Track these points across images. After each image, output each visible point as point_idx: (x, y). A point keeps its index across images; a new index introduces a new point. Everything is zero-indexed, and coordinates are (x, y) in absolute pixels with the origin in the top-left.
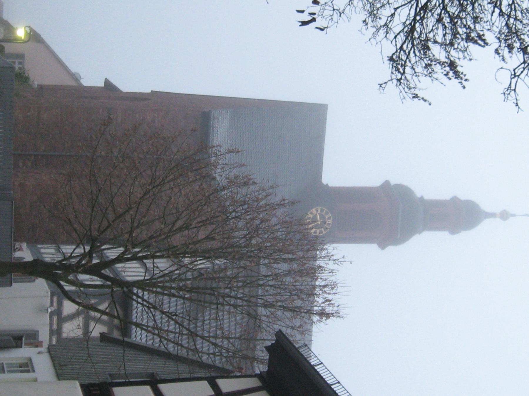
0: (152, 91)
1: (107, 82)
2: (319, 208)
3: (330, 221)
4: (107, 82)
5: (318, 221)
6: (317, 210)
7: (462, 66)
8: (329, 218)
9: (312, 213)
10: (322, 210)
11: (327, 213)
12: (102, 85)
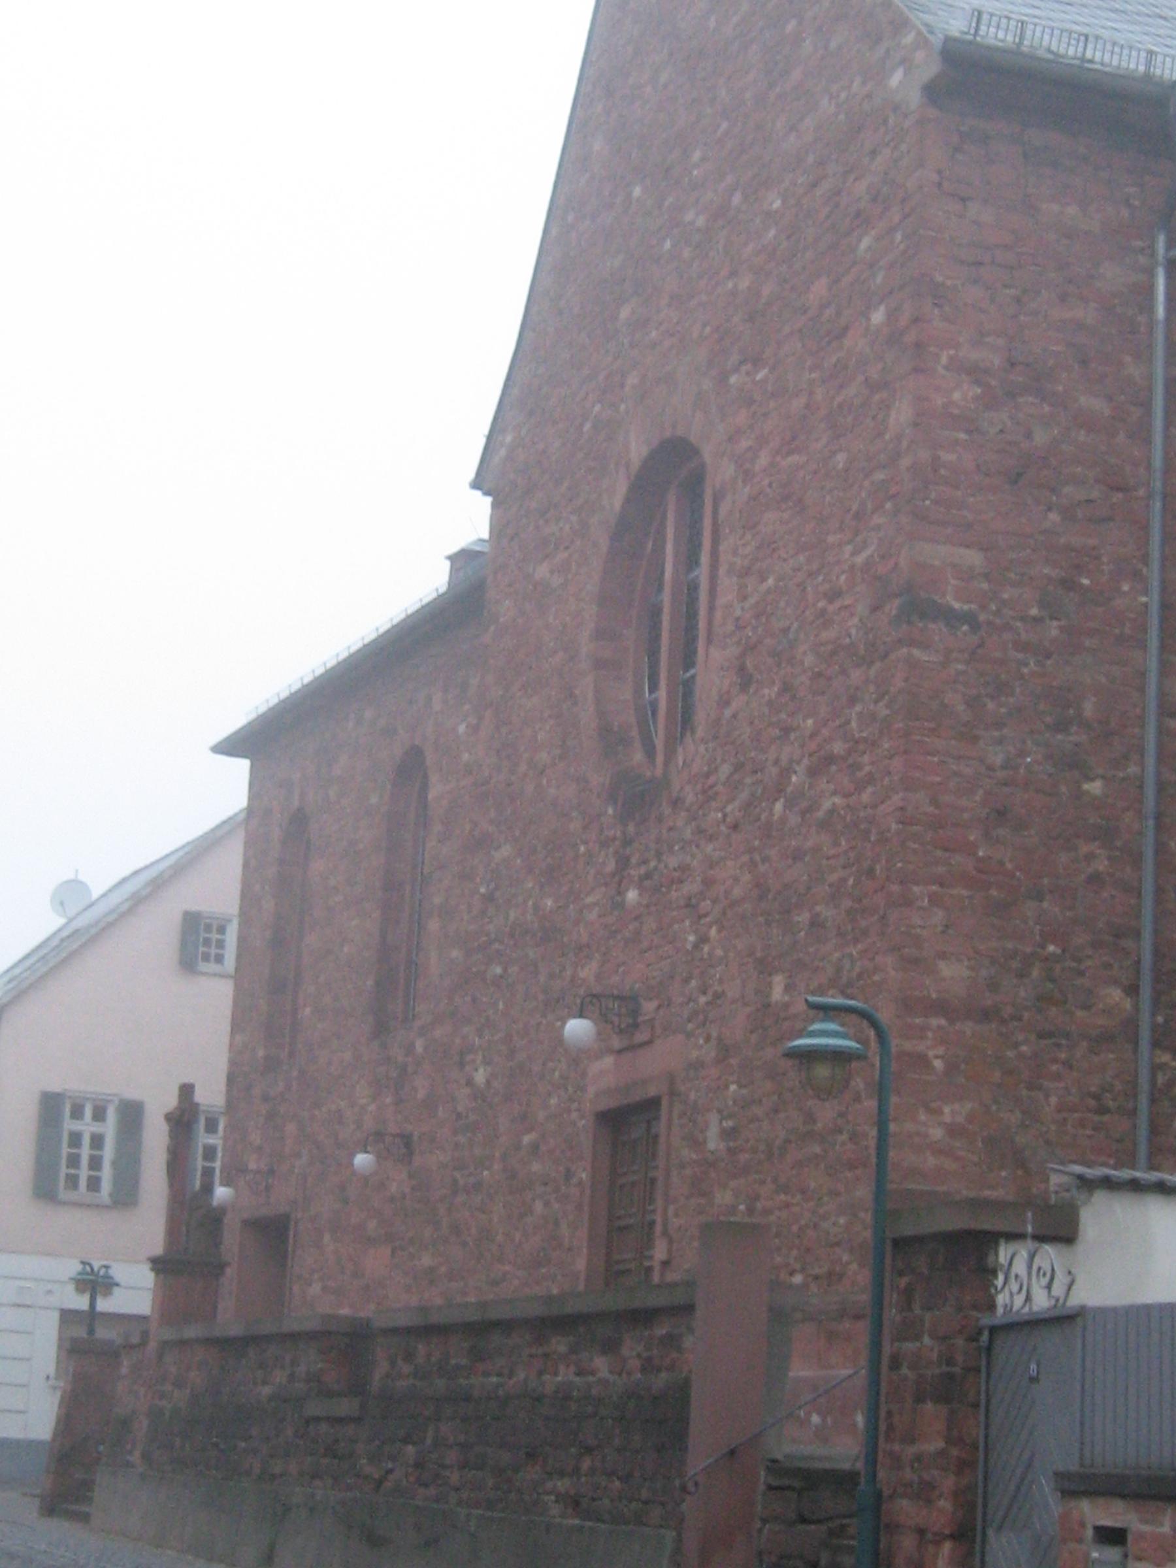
0: (476, 485)
1: (230, 747)
4: (230, 747)
12: (242, 766)
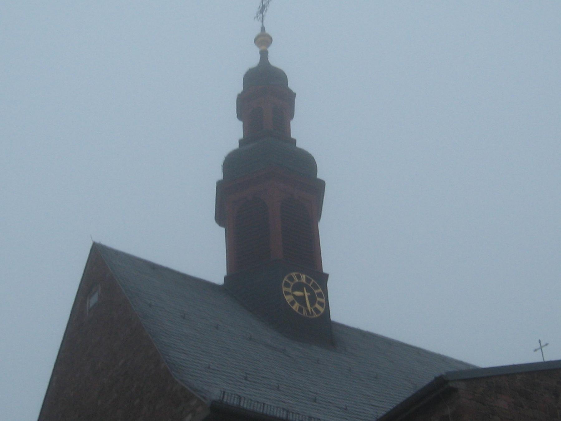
0: (327, 276)
2: (284, 289)
3: (304, 277)
5: (304, 297)
6: (287, 293)
7: (540, 342)
8: (299, 277)
9: (293, 303)
10: (287, 285)
11: (291, 279)
